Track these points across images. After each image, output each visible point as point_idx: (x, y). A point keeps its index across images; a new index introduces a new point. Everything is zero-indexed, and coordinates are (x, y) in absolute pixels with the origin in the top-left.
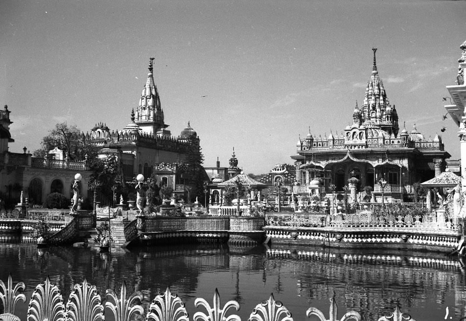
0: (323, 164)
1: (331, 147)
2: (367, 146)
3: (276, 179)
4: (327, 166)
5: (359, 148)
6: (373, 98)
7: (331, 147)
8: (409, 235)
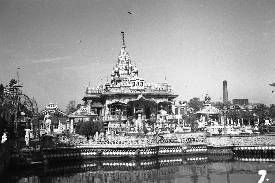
0: (126, 101)
1: (122, 91)
2: (145, 91)
3: (181, 109)
4: (129, 103)
5: (135, 92)
6: (125, 62)
7: (122, 91)
8: (103, 150)
